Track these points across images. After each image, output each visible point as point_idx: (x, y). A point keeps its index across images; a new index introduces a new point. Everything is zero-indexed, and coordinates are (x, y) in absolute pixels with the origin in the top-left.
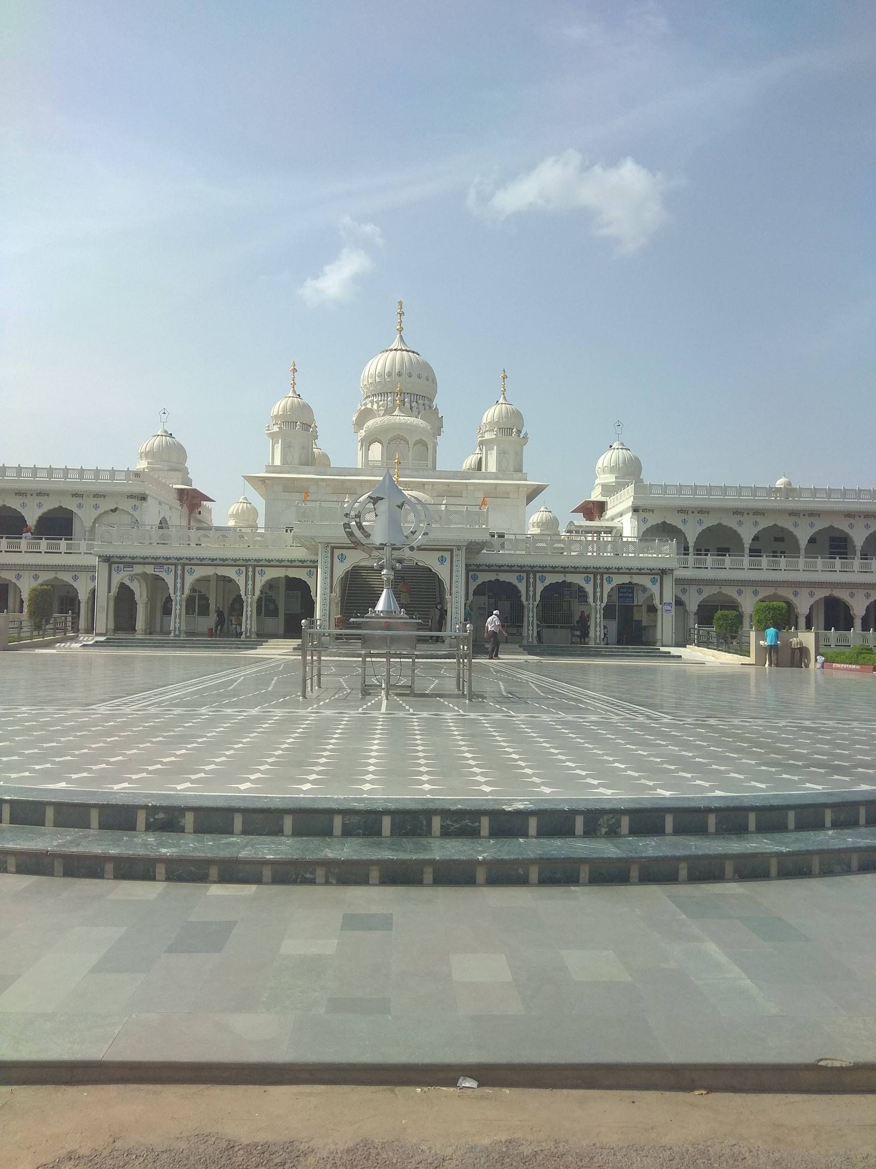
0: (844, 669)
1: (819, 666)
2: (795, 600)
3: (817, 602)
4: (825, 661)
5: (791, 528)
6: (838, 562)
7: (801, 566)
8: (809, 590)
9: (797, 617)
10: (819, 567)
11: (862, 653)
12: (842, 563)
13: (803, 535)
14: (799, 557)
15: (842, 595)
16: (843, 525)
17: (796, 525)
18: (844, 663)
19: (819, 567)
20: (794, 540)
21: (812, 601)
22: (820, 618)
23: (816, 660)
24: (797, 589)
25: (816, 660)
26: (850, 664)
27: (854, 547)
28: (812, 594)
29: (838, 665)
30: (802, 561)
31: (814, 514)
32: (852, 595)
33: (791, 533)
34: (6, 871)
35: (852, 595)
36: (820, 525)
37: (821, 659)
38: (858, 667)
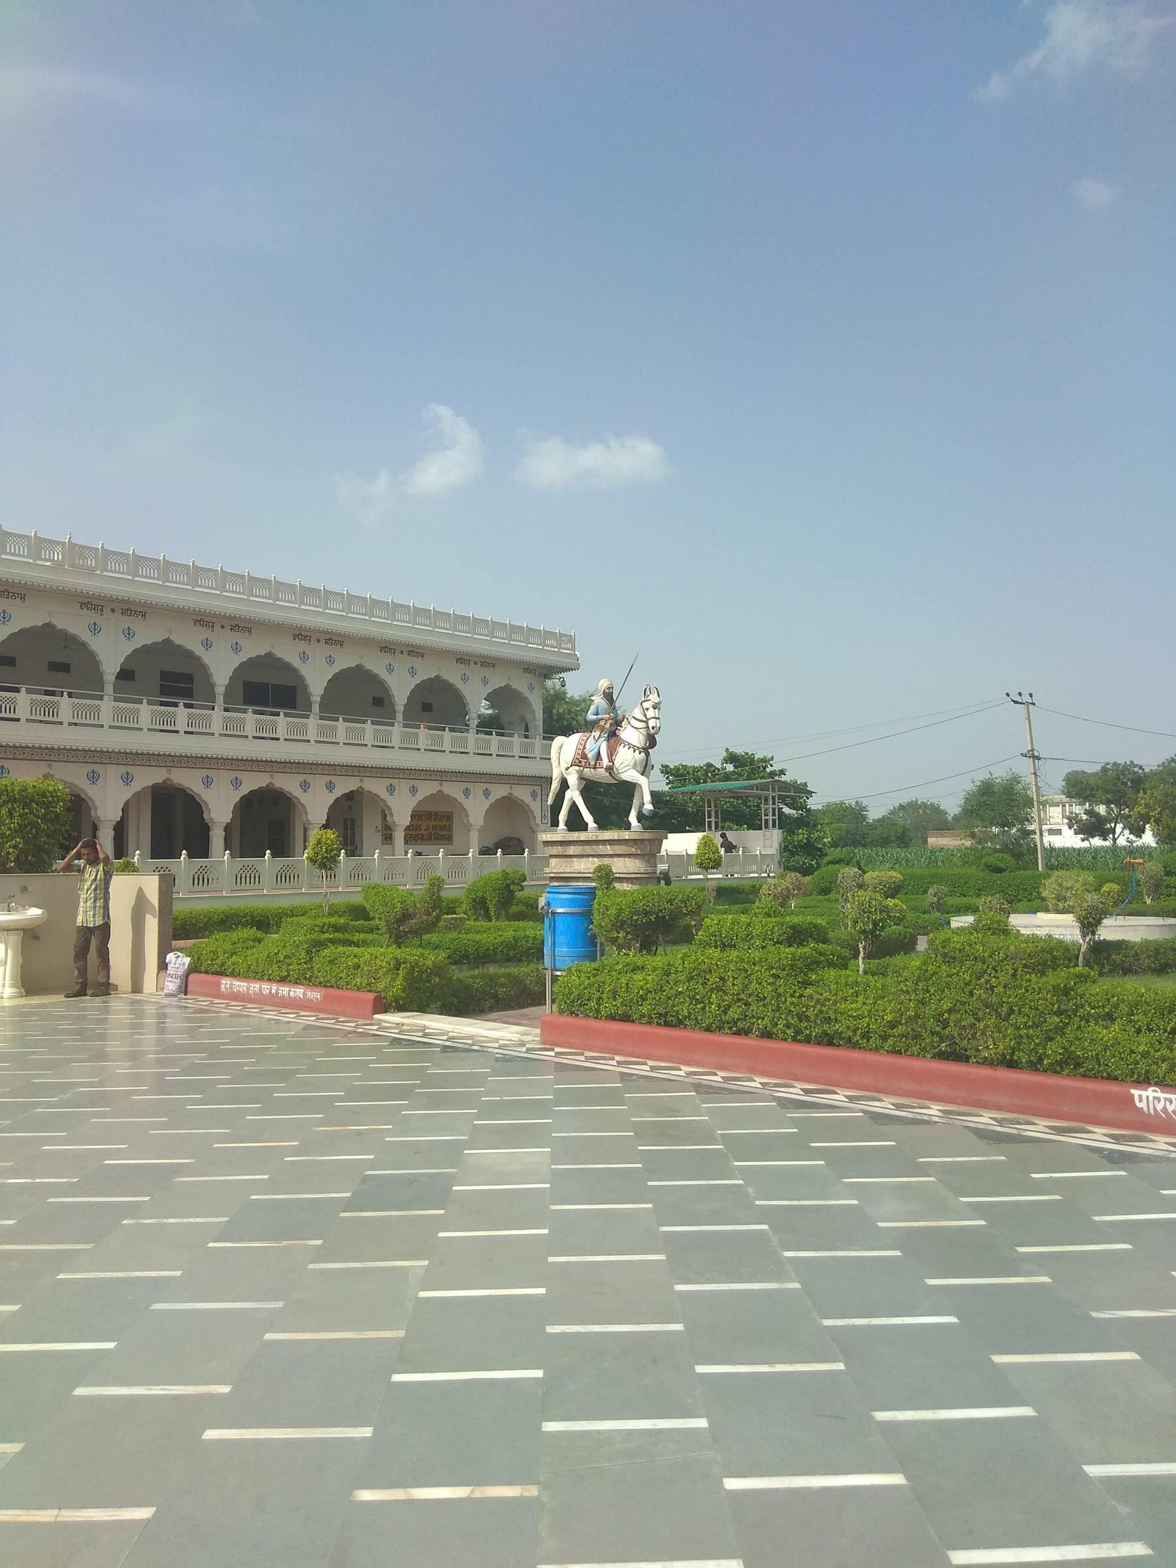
0: (262, 1000)
1: (171, 985)
2: (92, 792)
3: (137, 795)
4: (193, 969)
5: (86, 636)
6: (181, 714)
7: (106, 717)
8: (123, 769)
9: (95, 828)
10: (145, 721)
11: (320, 944)
12: (190, 716)
13: (111, 651)
14: (101, 698)
15: (189, 780)
16: (189, 639)
17: (95, 629)
18: (259, 976)
19: (145, 721)
20: (92, 662)
21: (127, 793)
22: (142, 832)
23: (163, 966)
24: (97, 768)
25: (163, 966)
26: (283, 980)
27: (212, 686)
28: (127, 779)
29: (240, 986)
30: (107, 707)
31: (132, 609)
32: (207, 782)
33: (83, 646)
34: (6, 871)
35: (207, 782)
36: (148, 634)
37: (178, 962)
38: (315, 995)
